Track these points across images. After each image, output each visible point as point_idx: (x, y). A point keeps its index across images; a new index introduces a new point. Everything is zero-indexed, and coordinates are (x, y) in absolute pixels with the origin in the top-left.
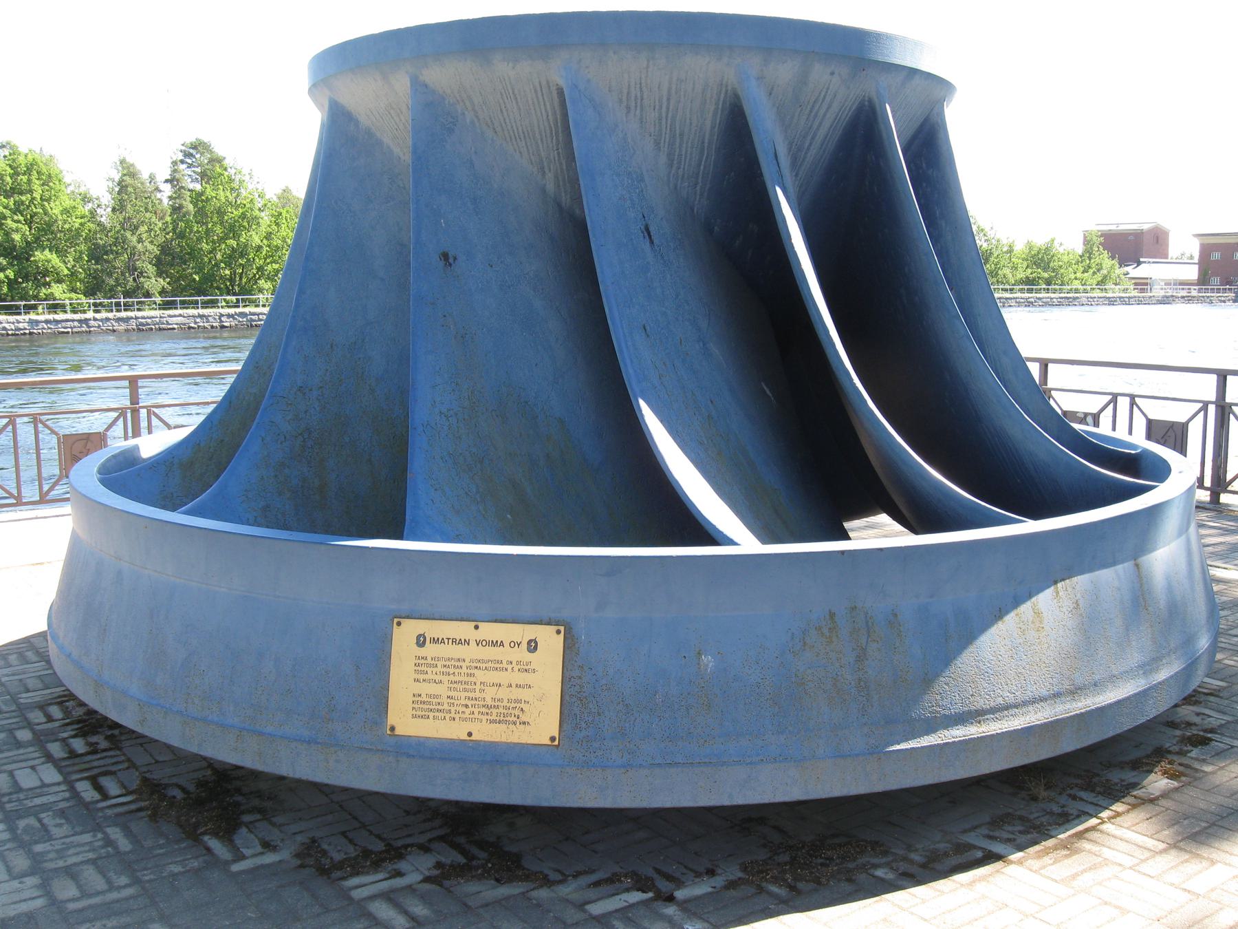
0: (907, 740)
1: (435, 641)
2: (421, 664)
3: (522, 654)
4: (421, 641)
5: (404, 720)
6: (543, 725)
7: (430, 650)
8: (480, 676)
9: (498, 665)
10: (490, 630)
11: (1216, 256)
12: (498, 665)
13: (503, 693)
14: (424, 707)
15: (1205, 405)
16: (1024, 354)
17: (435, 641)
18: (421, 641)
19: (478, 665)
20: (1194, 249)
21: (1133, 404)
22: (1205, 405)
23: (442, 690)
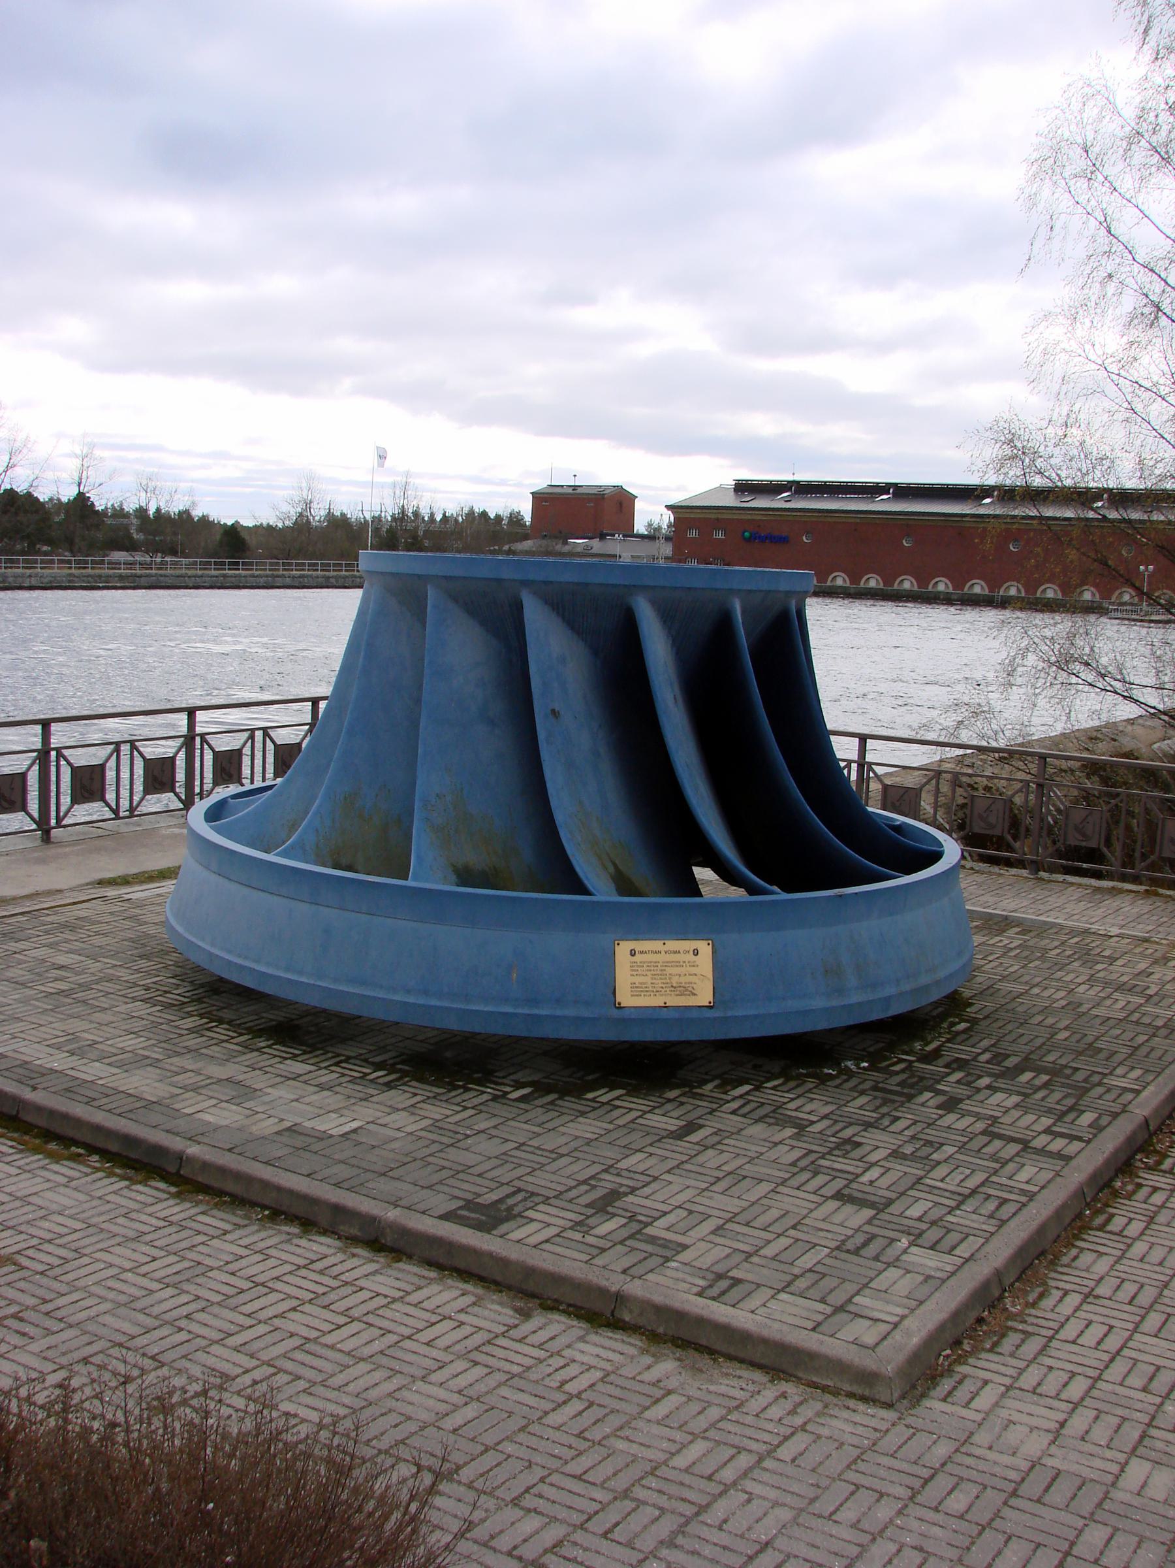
0: (1169, 889)
1: (641, 952)
2: (633, 967)
3: (691, 957)
4: (633, 953)
5: (625, 998)
6: (705, 996)
7: (638, 958)
8: (669, 970)
9: (678, 964)
10: (672, 945)
11: (693, 534)
12: (678, 964)
13: (683, 979)
14: (637, 990)
15: (59, 825)
16: (829, 727)
17: (641, 952)
18: (633, 953)
19: (667, 964)
20: (666, 519)
21: (116, 812)
22: (59, 825)
23: (648, 980)
